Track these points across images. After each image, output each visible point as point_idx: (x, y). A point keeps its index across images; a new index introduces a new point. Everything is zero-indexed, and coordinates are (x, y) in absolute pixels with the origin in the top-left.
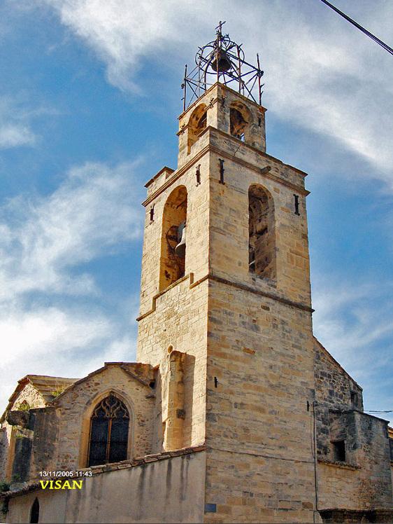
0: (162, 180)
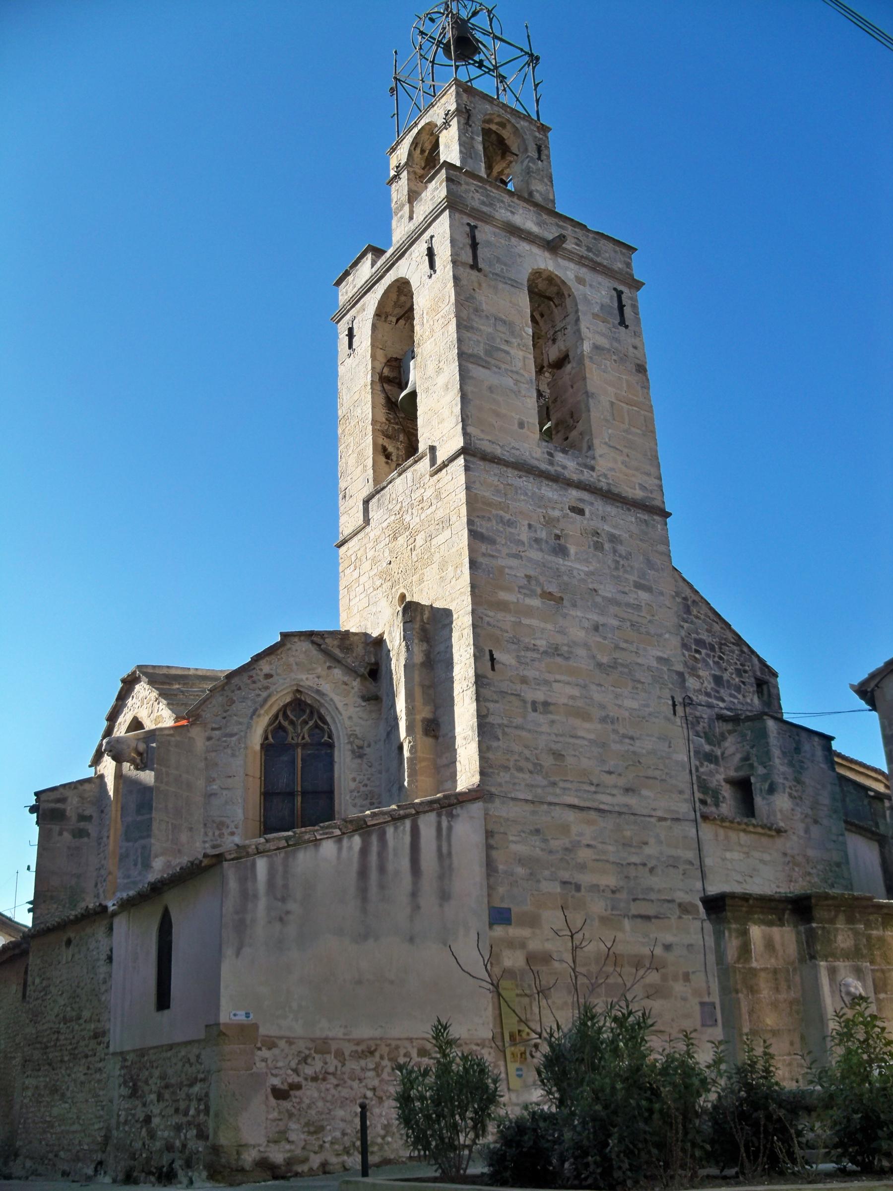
0: (365, 270)
